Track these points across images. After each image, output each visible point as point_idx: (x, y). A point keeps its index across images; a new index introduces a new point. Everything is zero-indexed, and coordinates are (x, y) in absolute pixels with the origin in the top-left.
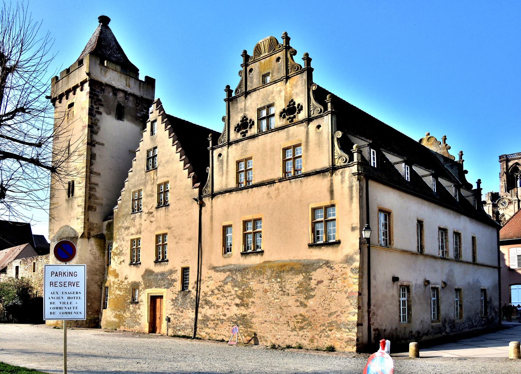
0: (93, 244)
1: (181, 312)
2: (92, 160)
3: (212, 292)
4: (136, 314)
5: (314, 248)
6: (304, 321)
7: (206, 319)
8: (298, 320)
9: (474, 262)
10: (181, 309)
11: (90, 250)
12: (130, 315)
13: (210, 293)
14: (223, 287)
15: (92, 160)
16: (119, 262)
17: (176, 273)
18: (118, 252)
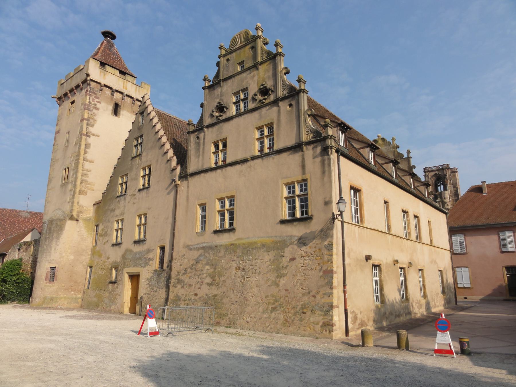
0: (82, 225)
1: (155, 292)
2: (86, 149)
3: (184, 270)
4: (113, 294)
5: (287, 224)
6: (277, 302)
7: (177, 300)
8: (270, 301)
9: (431, 244)
10: (155, 289)
11: (78, 232)
12: (108, 294)
13: (183, 272)
14: (195, 265)
15: (86, 149)
16: (104, 243)
17: (153, 252)
18: (103, 233)
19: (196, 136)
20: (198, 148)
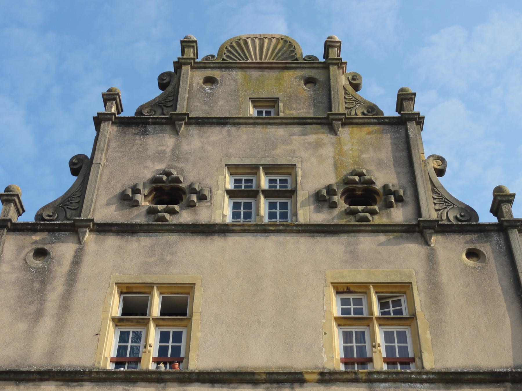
19: (35, 247)
20: (37, 285)
